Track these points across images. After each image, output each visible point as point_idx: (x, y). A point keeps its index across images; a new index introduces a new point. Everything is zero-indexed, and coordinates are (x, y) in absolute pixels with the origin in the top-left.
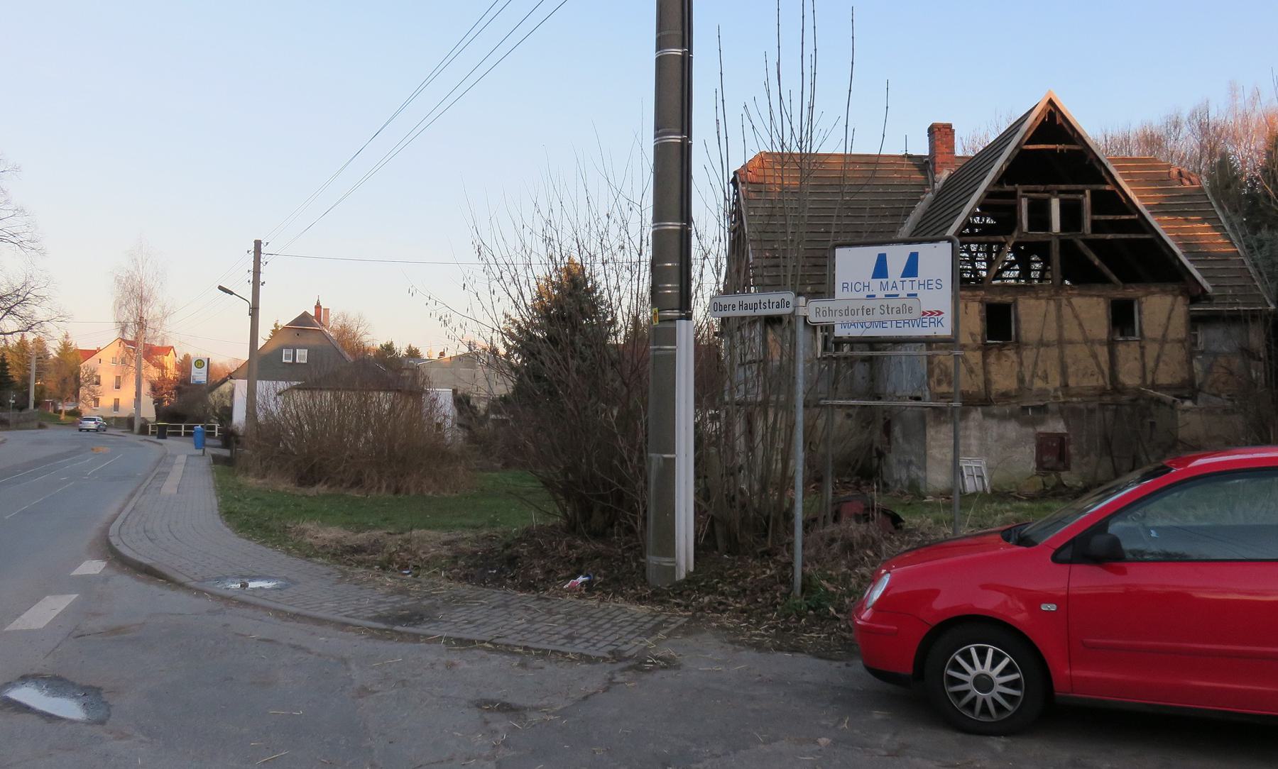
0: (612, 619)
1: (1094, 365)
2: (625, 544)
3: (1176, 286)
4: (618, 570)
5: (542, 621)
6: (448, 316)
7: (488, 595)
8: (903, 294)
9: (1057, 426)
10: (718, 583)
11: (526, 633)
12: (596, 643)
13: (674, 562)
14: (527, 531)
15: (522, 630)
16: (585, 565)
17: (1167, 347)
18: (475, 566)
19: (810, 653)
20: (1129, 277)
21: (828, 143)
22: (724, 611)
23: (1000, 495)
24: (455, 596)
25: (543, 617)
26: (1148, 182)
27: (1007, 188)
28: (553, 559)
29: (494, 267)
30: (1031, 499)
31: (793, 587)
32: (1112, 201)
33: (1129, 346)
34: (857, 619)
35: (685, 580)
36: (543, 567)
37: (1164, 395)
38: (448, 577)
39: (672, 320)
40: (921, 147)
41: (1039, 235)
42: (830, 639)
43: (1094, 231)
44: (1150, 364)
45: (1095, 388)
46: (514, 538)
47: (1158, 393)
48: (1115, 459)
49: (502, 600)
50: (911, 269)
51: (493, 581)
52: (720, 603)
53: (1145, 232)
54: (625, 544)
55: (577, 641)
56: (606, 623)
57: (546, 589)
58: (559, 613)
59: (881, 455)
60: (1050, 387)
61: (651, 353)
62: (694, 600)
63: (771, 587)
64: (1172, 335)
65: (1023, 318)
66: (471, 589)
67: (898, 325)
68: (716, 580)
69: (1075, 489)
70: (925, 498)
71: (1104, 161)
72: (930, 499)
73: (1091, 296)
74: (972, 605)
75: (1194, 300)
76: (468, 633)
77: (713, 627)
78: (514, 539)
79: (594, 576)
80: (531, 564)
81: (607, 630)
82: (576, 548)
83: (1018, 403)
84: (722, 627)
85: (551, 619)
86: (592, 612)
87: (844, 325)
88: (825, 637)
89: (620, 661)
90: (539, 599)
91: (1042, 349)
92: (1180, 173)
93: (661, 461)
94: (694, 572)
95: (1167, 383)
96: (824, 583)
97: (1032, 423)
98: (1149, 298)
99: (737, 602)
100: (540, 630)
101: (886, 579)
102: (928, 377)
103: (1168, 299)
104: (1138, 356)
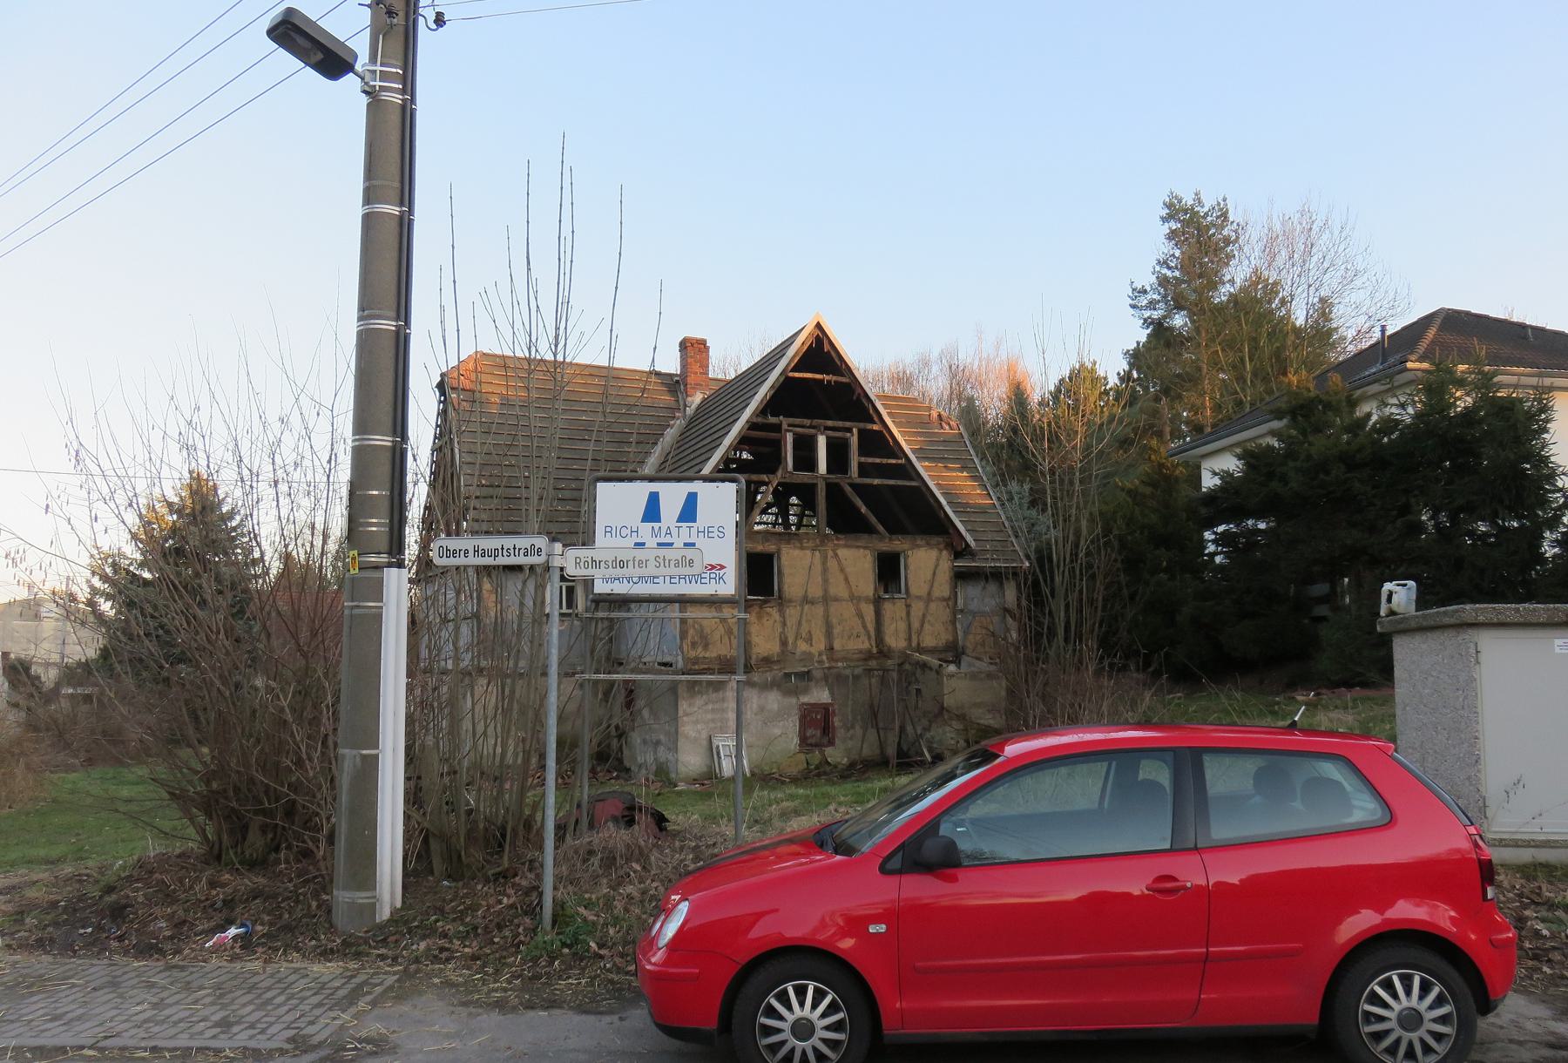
0: (286, 989)
1: (860, 625)
2: (299, 876)
3: (941, 539)
4: (289, 913)
5: (177, 1003)
6: (21, 552)
7: (83, 970)
8: (679, 543)
9: (822, 696)
10: (437, 921)
11: (151, 1025)
12: (267, 1028)
13: (375, 897)
14: (141, 864)
15: (145, 1021)
16: (238, 910)
17: (933, 606)
18: (56, 924)
19: (571, 1008)
20: (895, 529)
21: (587, 351)
22: (448, 960)
23: (764, 778)
24: (24, 976)
25: (178, 997)
26: (909, 424)
27: (772, 420)
28: (186, 906)
29: (99, 480)
30: (795, 781)
31: (541, 918)
32: (878, 443)
33: (894, 604)
34: (644, 962)
35: (388, 921)
36: (170, 918)
37: (929, 659)
38: (9, 946)
39: (378, 567)
40: (670, 363)
41: (804, 477)
42: (593, 985)
43: (861, 475)
44: (916, 625)
45: (861, 652)
46: (119, 876)
47: (924, 657)
48: (881, 731)
49: (107, 975)
50: (689, 512)
51: (87, 946)
52: (442, 949)
53: (912, 479)
54: (299, 876)
55: (235, 1029)
56: (279, 994)
57: (177, 952)
58: (201, 988)
59: (621, 734)
60: (814, 650)
61: (347, 612)
62: (404, 948)
63: (511, 922)
64: (937, 593)
65: (786, 571)
66: (51, 964)
67: (673, 580)
68: (433, 918)
69: (840, 767)
70: (676, 786)
71: (873, 398)
72: (681, 787)
73: (858, 547)
74: (780, 933)
75: (958, 555)
76: (53, 1036)
77: (435, 985)
78: (120, 878)
79: (253, 926)
80: (151, 915)
81: (279, 1006)
82: (223, 885)
83: (780, 670)
84: (448, 984)
85: (190, 1000)
86: (255, 979)
87: (606, 580)
88: (586, 982)
89: (305, 1052)
90: (170, 968)
91: (806, 607)
92: (940, 416)
93: (358, 759)
94: (402, 909)
95: (933, 645)
96: (581, 910)
97: (795, 692)
98: (915, 551)
99: (465, 946)
100: (175, 1018)
101: (684, 907)
102: (681, 639)
103: (934, 553)
104: (904, 615)
